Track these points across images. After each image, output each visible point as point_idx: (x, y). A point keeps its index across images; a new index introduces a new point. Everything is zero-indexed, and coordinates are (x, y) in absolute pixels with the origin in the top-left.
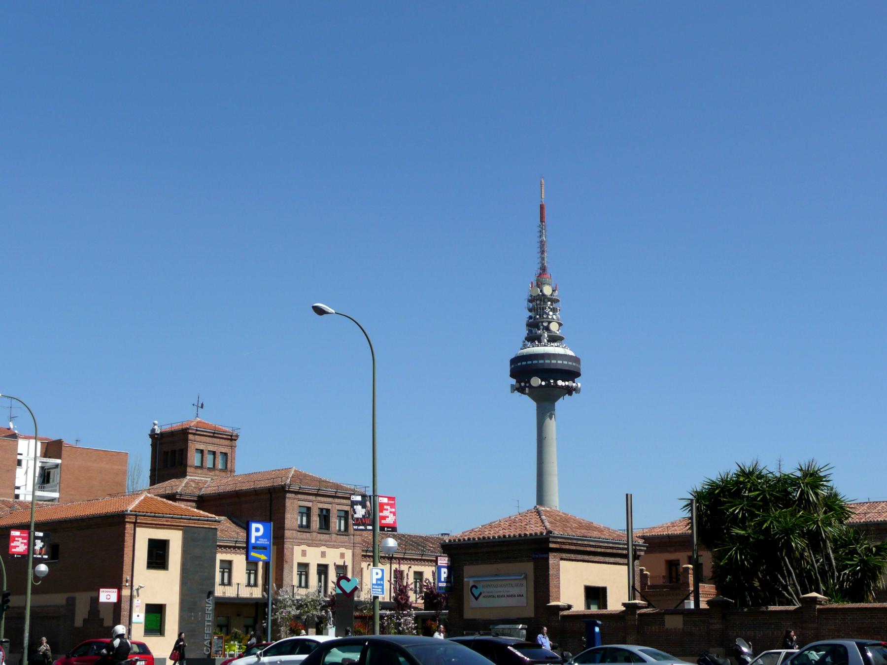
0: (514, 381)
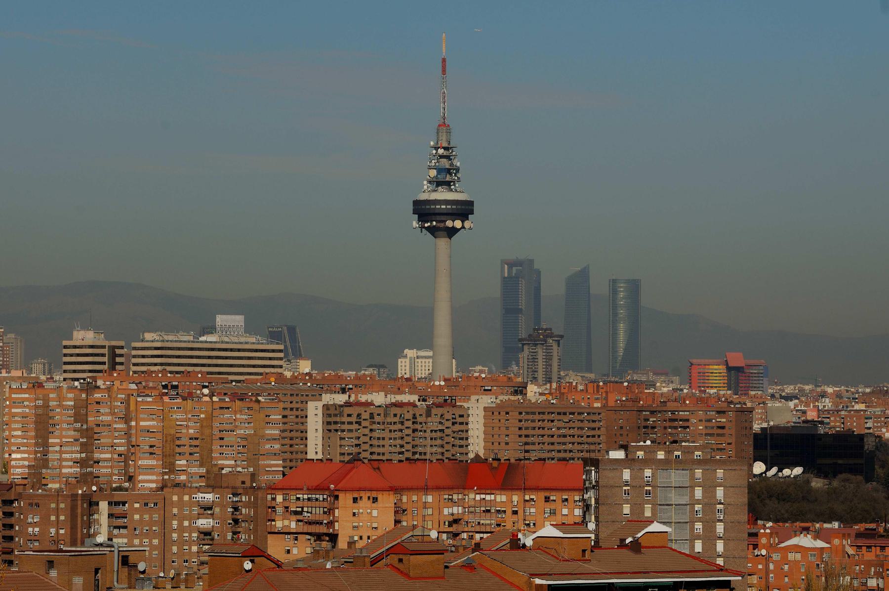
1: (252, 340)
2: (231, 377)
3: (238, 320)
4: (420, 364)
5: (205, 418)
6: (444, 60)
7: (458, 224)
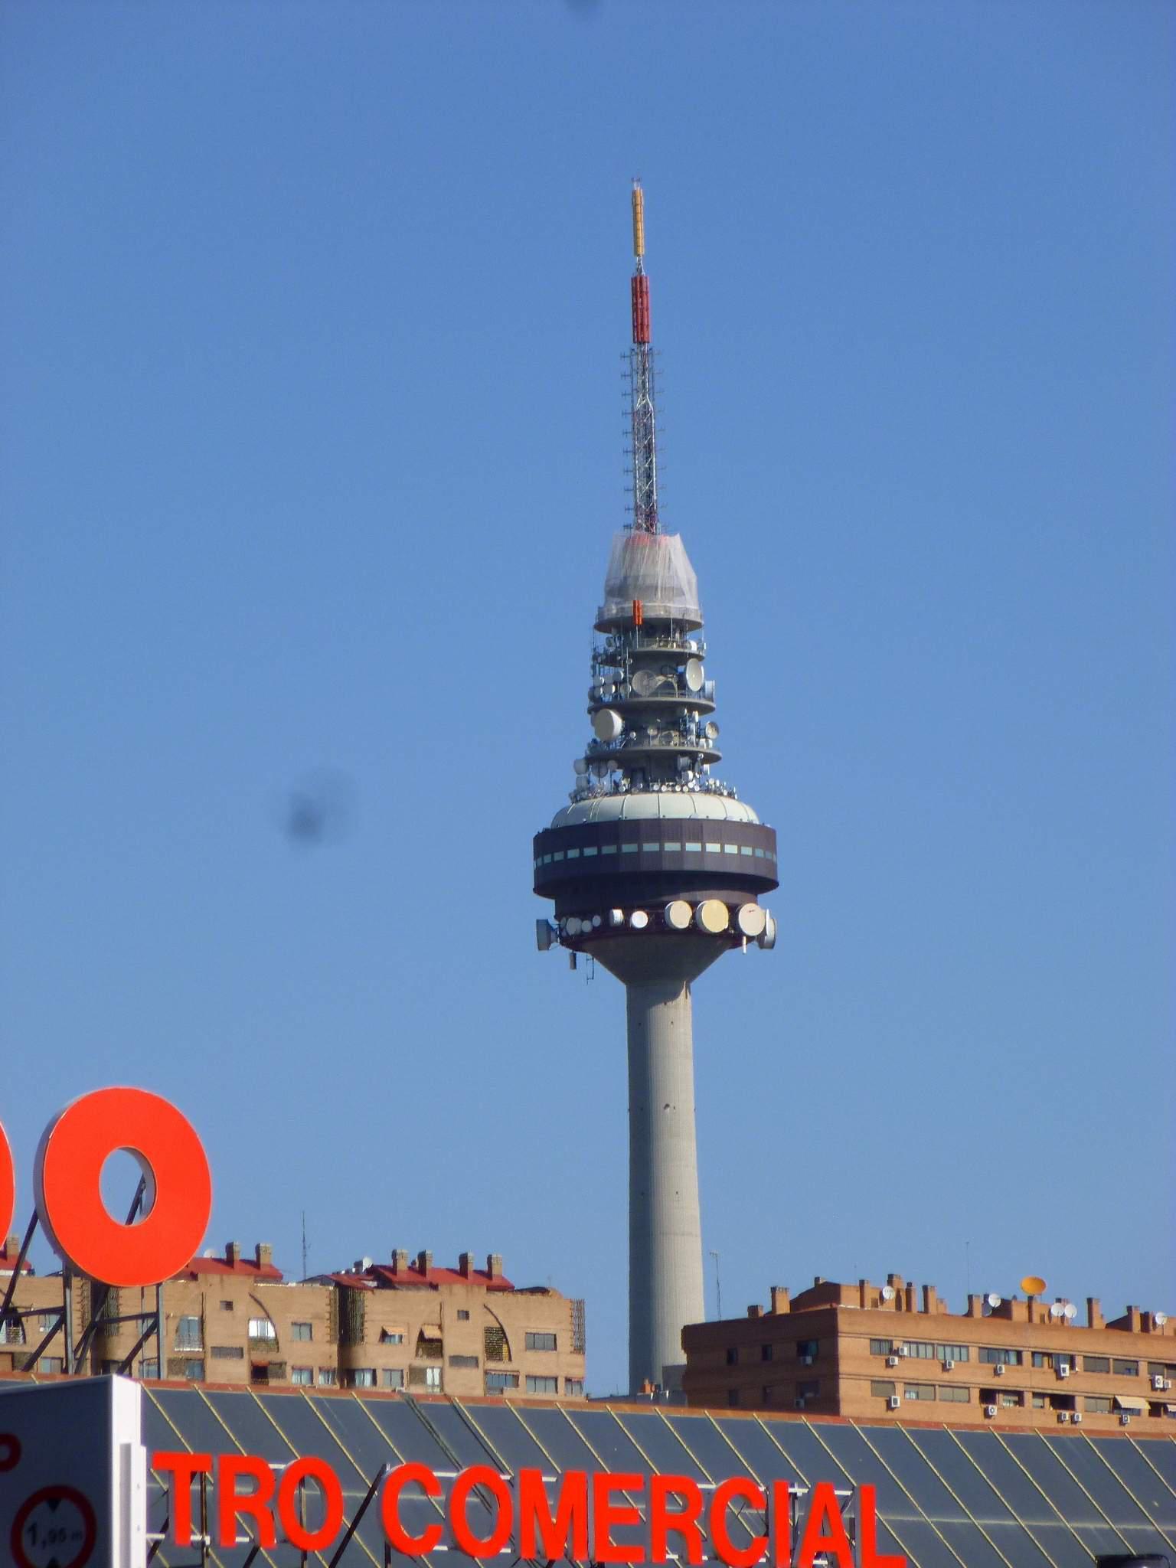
0: (547, 908)
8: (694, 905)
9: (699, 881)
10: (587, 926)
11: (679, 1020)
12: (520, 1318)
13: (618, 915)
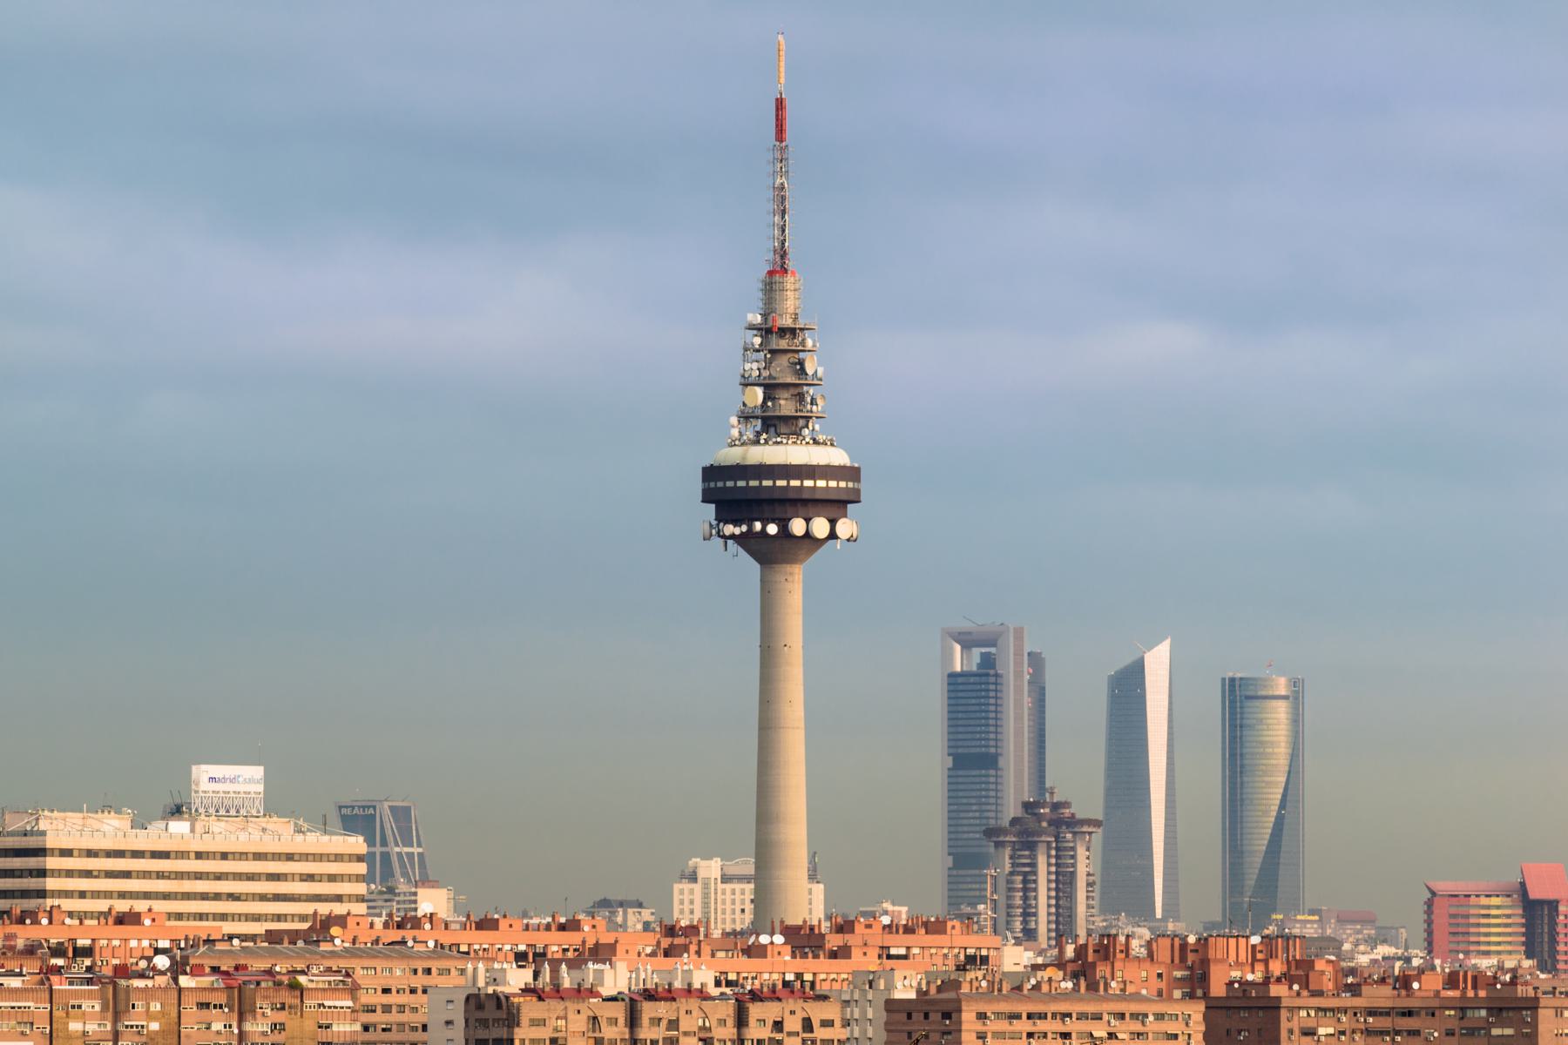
1: (281, 835)
2: (229, 927)
3: (248, 779)
4: (728, 897)
5: (162, 1032)
6: (780, 104)
7: (820, 527)
8: (808, 520)
9: (809, 504)
10: (737, 531)
11: (795, 582)
12: (818, 1012)
13: (758, 526)
